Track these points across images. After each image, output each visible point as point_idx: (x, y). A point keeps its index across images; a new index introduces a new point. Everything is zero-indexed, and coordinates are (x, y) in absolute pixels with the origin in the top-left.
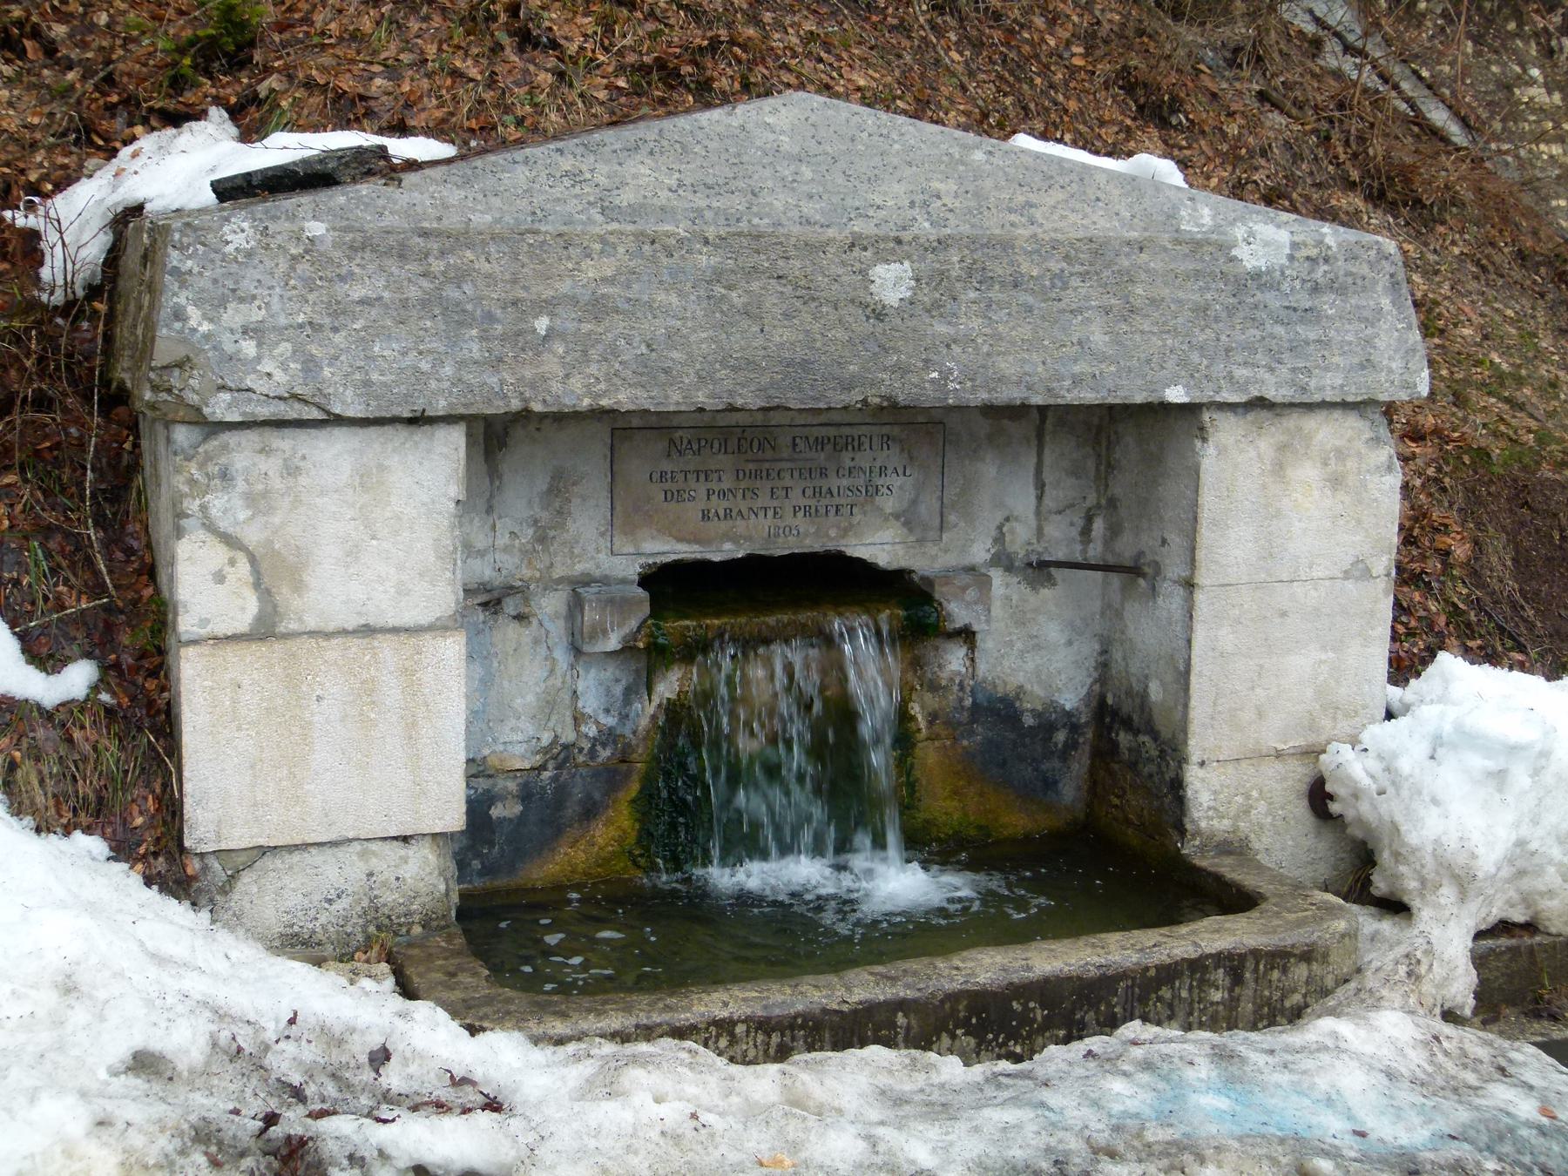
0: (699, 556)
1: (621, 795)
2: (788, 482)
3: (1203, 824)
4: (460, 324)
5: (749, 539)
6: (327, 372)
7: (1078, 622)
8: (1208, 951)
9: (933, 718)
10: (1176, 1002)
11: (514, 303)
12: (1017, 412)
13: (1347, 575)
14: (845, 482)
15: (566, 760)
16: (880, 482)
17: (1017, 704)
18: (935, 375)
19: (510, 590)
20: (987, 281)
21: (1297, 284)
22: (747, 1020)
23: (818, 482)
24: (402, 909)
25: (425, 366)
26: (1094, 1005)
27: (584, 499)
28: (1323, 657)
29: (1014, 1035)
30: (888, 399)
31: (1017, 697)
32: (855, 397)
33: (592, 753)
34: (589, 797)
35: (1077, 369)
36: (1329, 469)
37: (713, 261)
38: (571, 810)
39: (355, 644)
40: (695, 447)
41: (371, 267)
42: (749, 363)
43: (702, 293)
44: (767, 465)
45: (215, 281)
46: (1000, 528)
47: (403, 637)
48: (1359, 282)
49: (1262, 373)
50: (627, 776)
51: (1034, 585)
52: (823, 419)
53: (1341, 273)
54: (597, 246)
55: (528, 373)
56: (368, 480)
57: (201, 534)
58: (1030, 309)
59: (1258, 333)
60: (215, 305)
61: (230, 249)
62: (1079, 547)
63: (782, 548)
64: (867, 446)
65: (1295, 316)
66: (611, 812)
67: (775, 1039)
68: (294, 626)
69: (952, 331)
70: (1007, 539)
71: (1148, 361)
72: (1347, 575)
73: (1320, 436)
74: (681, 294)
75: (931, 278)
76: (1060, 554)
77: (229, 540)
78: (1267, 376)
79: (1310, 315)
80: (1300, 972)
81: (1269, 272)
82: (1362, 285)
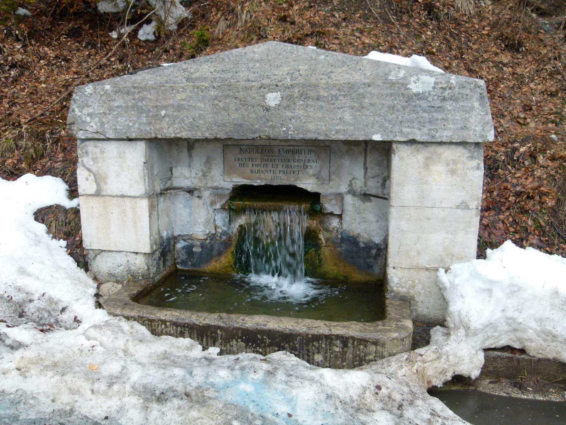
0: (250, 183)
1: (229, 250)
2: (277, 163)
3: (395, 289)
4: (141, 113)
5: (265, 179)
6: (106, 126)
7: (380, 215)
8: (333, 333)
9: (327, 240)
10: (320, 348)
11: (156, 107)
12: (356, 143)
13: (458, 207)
14: (296, 164)
15: (213, 238)
16: (308, 164)
17: (358, 239)
18: (285, 129)
19: (195, 189)
20: (307, 98)
21: (436, 98)
22: (170, 321)
23: (287, 164)
24: (136, 272)
25: (131, 124)
26: (288, 342)
27: (216, 165)
28: (447, 236)
29: (258, 345)
30: (268, 136)
31: (358, 237)
32: (257, 135)
33: (221, 237)
34: (220, 249)
35: (338, 128)
36: (449, 167)
37: (216, 93)
38: (215, 252)
39: (120, 199)
40: (248, 151)
41: (120, 97)
42: (223, 124)
43: (211, 103)
44: (271, 157)
45: (82, 102)
46: (351, 181)
47: (132, 199)
48: (465, 97)
49: (415, 130)
50: (230, 245)
51: (363, 201)
52: (288, 144)
53: (457, 93)
54: (181, 90)
55: (158, 127)
56: (121, 156)
57: (82, 168)
58: (322, 107)
59: (415, 116)
60: (81, 108)
61: (86, 93)
62: (380, 190)
63: (275, 183)
64: (303, 153)
65: (433, 110)
66: (226, 254)
67: (179, 329)
68: (105, 193)
69: (292, 114)
70: (354, 185)
71: (367, 126)
72: (458, 207)
73: (445, 155)
74: (205, 104)
75: (287, 97)
76: (373, 192)
77: (89, 170)
78: (417, 131)
79: (440, 109)
80: (373, 348)
81: (423, 93)
82: (467, 98)
